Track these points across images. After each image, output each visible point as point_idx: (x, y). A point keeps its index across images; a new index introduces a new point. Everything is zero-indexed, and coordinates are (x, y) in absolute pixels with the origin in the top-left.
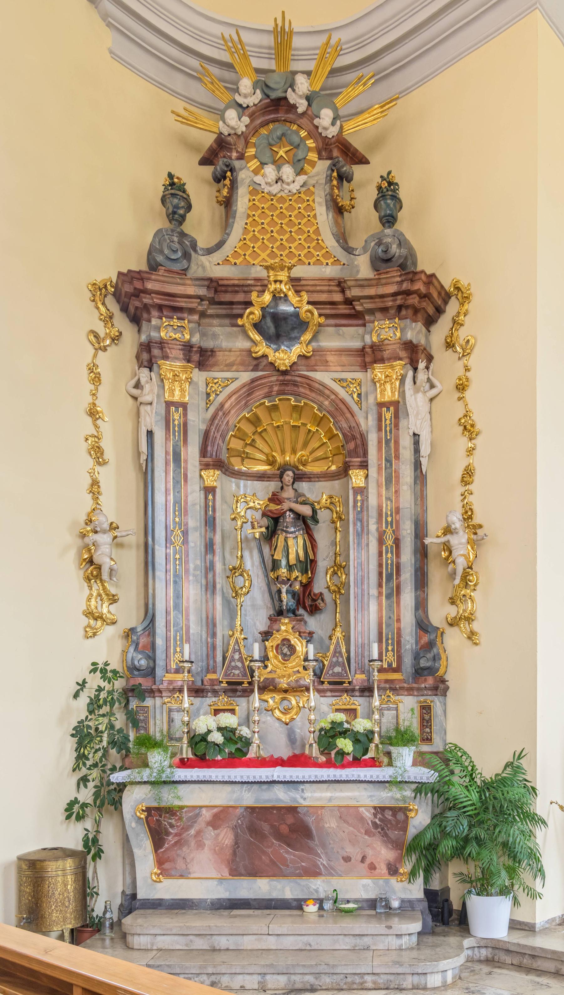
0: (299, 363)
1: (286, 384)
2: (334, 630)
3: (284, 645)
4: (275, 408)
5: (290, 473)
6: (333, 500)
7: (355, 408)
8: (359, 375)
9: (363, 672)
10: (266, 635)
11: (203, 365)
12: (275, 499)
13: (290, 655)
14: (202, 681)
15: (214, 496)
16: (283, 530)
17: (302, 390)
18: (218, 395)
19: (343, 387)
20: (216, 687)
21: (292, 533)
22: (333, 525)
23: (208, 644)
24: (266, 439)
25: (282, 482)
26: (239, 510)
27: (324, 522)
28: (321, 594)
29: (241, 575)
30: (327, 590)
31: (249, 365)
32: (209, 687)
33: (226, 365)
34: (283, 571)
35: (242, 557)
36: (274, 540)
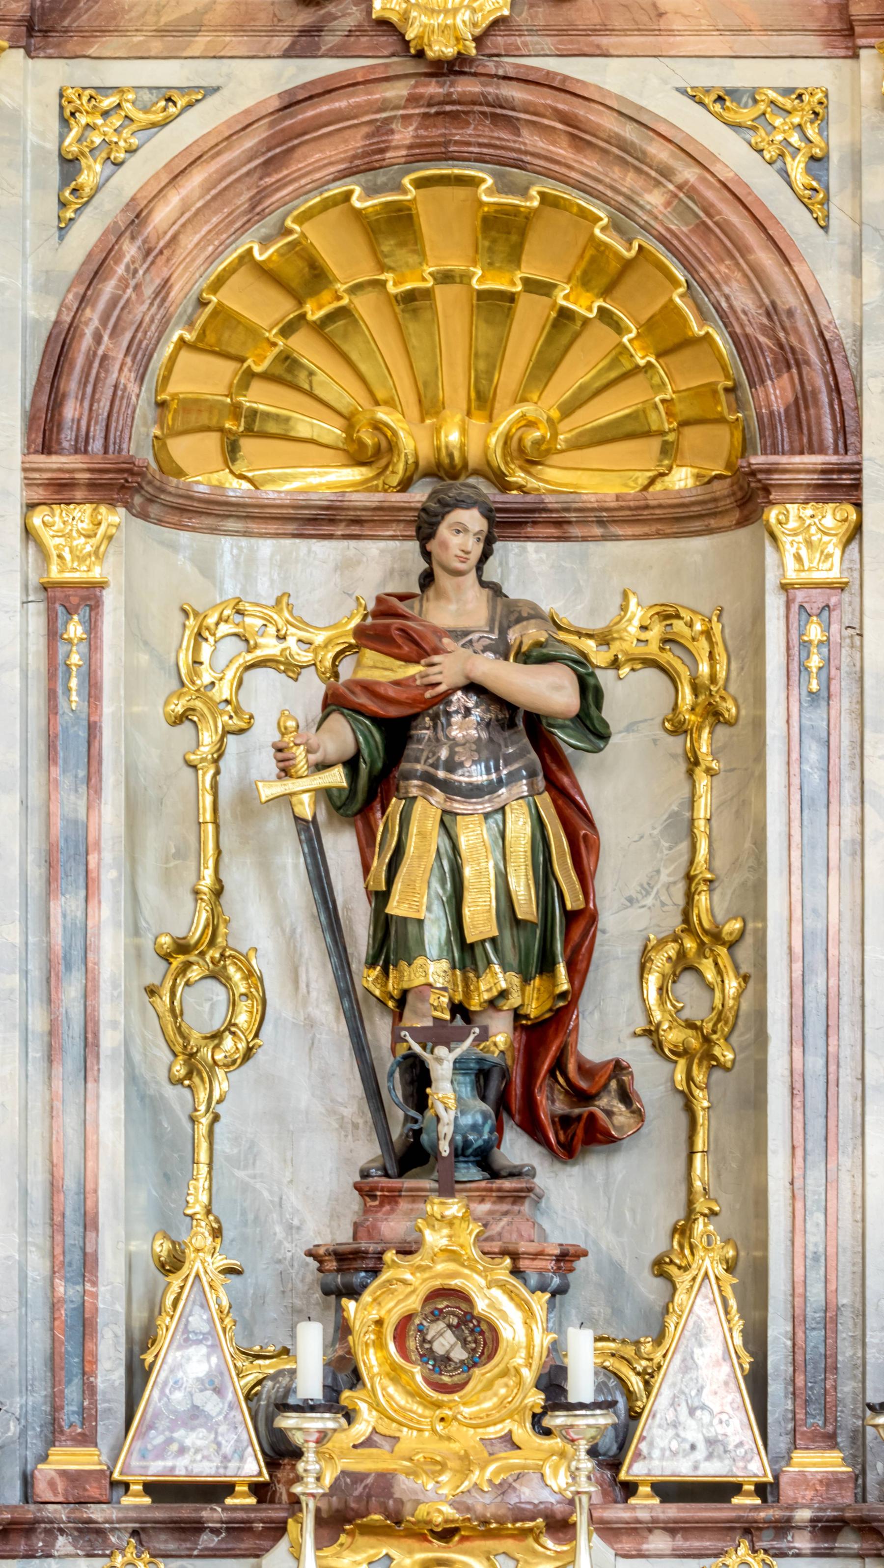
0: (523, 18)
1: (454, 116)
2: (683, 1230)
3: (437, 1315)
4: (398, 223)
6: (679, 626)
7: (795, 221)
8: (820, 74)
9: (830, 1440)
10: (347, 1270)
11: (45, 33)
12: (388, 627)
13: (471, 1364)
14: (27, 1481)
15: (93, 628)
17: (532, 141)
18: (118, 164)
19: (736, 126)
20: (97, 1513)
21: (474, 792)
22: (676, 744)
23: (53, 1307)
24: (363, 367)
27: (629, 729)
28: (618, 1068)
29: (217, 975)
30: (644, 1044)
31: (272, 32)
32: (60, 1513)
33: (162, 32)
34: (432, 970)
35: (218, 892)
36: (387, 821)
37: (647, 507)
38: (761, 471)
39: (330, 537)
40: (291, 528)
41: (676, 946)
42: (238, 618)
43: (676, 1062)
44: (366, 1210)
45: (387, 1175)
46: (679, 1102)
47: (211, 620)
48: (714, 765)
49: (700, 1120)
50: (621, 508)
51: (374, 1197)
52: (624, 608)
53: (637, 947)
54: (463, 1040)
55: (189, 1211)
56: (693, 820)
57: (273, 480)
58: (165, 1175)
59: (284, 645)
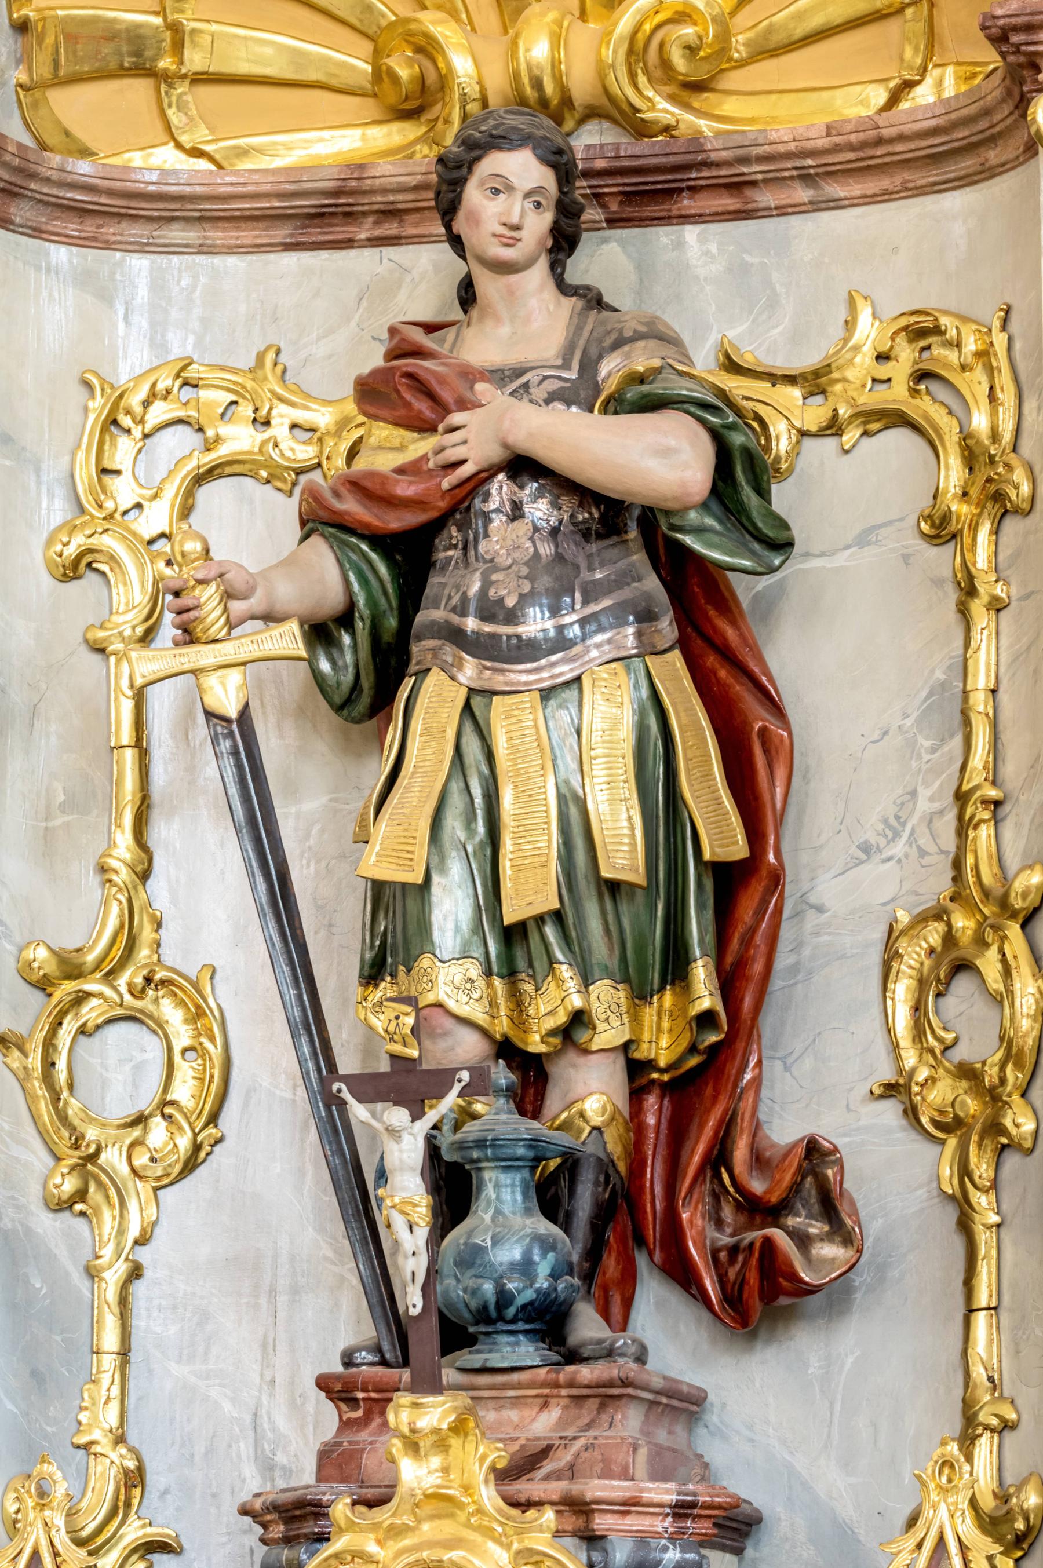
5: (522, 168)
12: (406, 385)
16: (456, 636)
22: (941, 560)
25: (457, 242)
26: (123, 491)
34: (454, 977)
37: (880, 141)
38: (1016, 29)
39: (348, 244)
40: (281, 233)
41: (941, 927)
42: (187, 393)
43: (942, 1142)
44: (345, 1425)
45: (384, 1363)
46: (951, 1214)
47: (135, 401)
48: (999, 590)
49: (982, 1251)
50: (836, 149)
51: (353, 1403)
52: (850, 325)
53: (879, 934)
54: (441, 1096)
55: (82, 1440)
56: (965, 693)
57: (243, 153)
58: (34, 1373)
59: (269, 433)
